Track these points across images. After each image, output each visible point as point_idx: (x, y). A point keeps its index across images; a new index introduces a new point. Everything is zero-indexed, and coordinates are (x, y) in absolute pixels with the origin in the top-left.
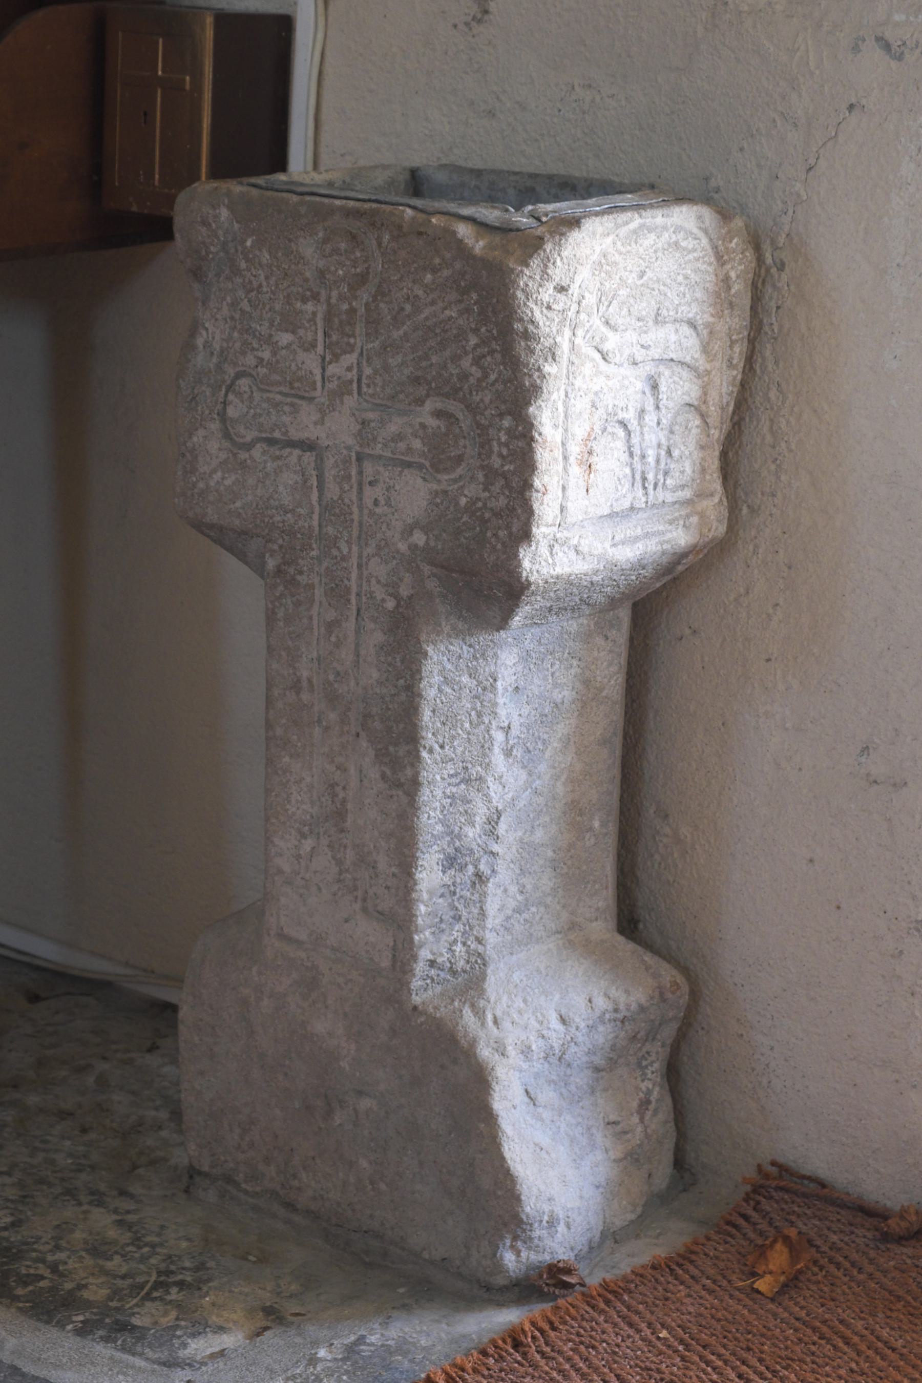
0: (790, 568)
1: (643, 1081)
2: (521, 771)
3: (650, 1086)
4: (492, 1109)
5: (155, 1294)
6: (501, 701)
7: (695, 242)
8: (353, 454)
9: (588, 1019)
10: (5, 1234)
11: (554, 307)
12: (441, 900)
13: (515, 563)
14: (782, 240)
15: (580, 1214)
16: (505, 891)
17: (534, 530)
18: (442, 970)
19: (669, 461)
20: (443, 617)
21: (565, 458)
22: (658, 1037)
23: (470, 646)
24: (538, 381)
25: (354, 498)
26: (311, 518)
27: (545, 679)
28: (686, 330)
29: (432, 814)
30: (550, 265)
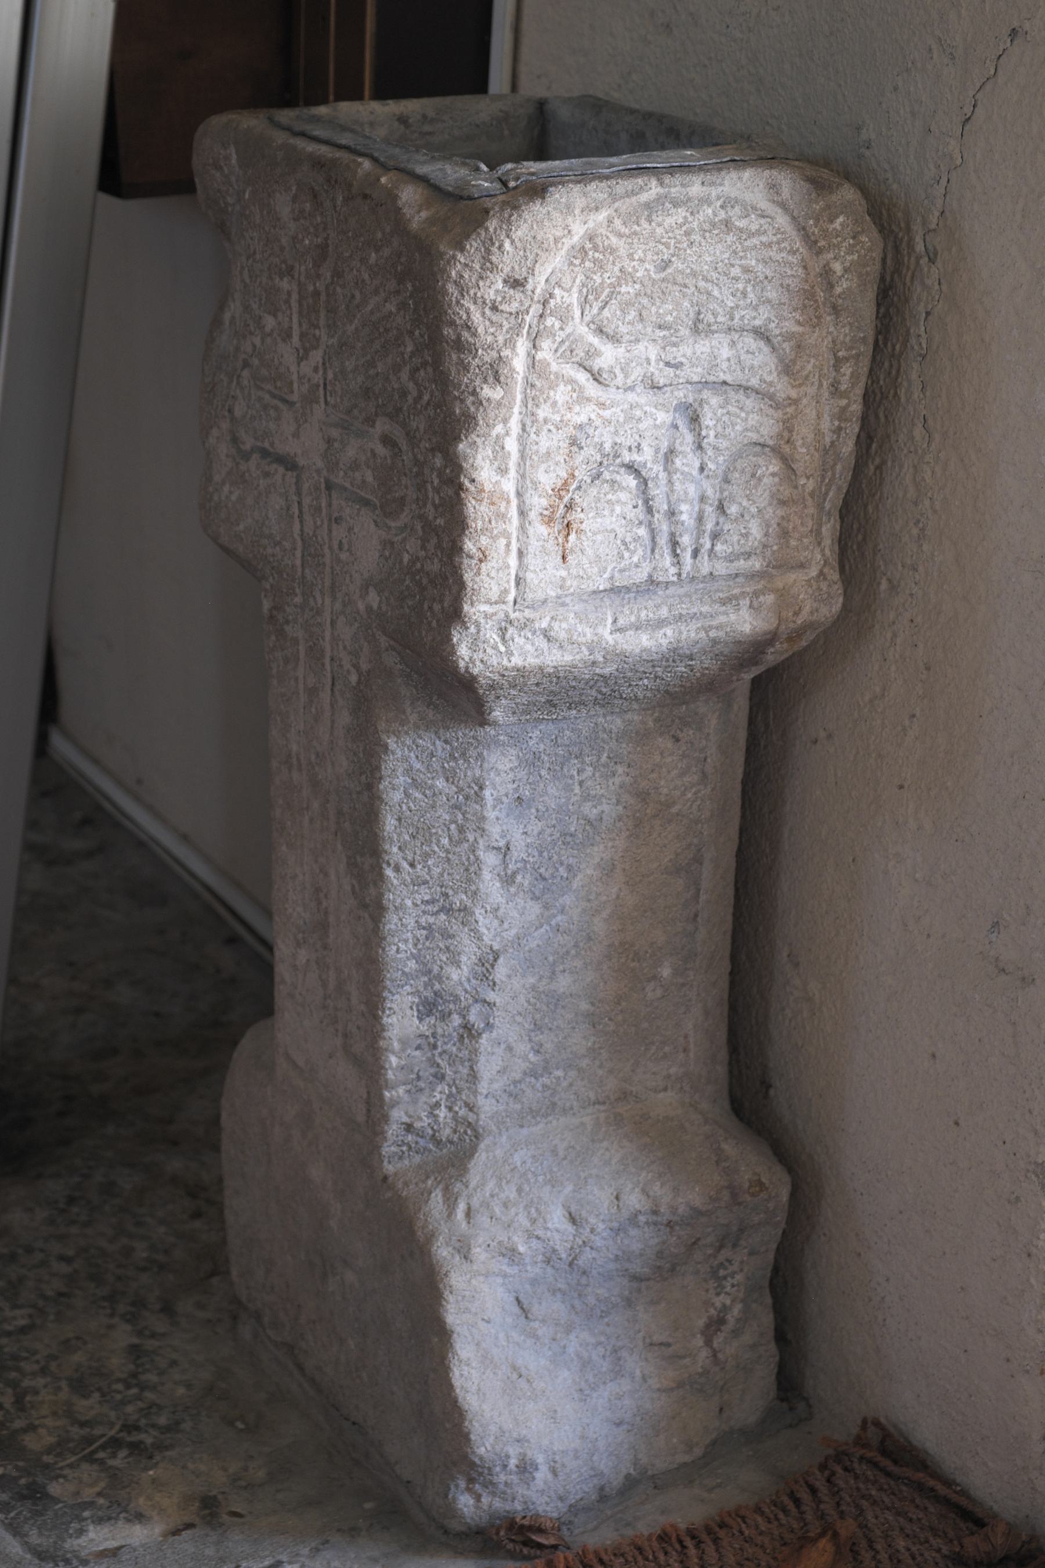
0: (928, 669)
1: (718, 1294)
2: (531, 903)
3: (728, 1302)
4: (445, 1323)
5: (101, 1455)
6: (491, 814)
7: (762, 221)
8: (322, 480)
9: (611, 1221)
10: (5, 1341)
11: (504, 307)
12: (417, 1053)
13: (449, 649)
14: (933, 219)
15: (577, 1458)
16: (510, 1048)
17: (466, 608)
18: (422, 1137)
19: (722, 520)
20: (408, 703)
21: (522, 513)
22: (743, 1243)
23: (446, 742)
24: (472, 409)
25: (326, 537)
26: (294, 555)
27: (568, 788)
28: (750, 342)
29: (402, 946)
30: (494, 249)
